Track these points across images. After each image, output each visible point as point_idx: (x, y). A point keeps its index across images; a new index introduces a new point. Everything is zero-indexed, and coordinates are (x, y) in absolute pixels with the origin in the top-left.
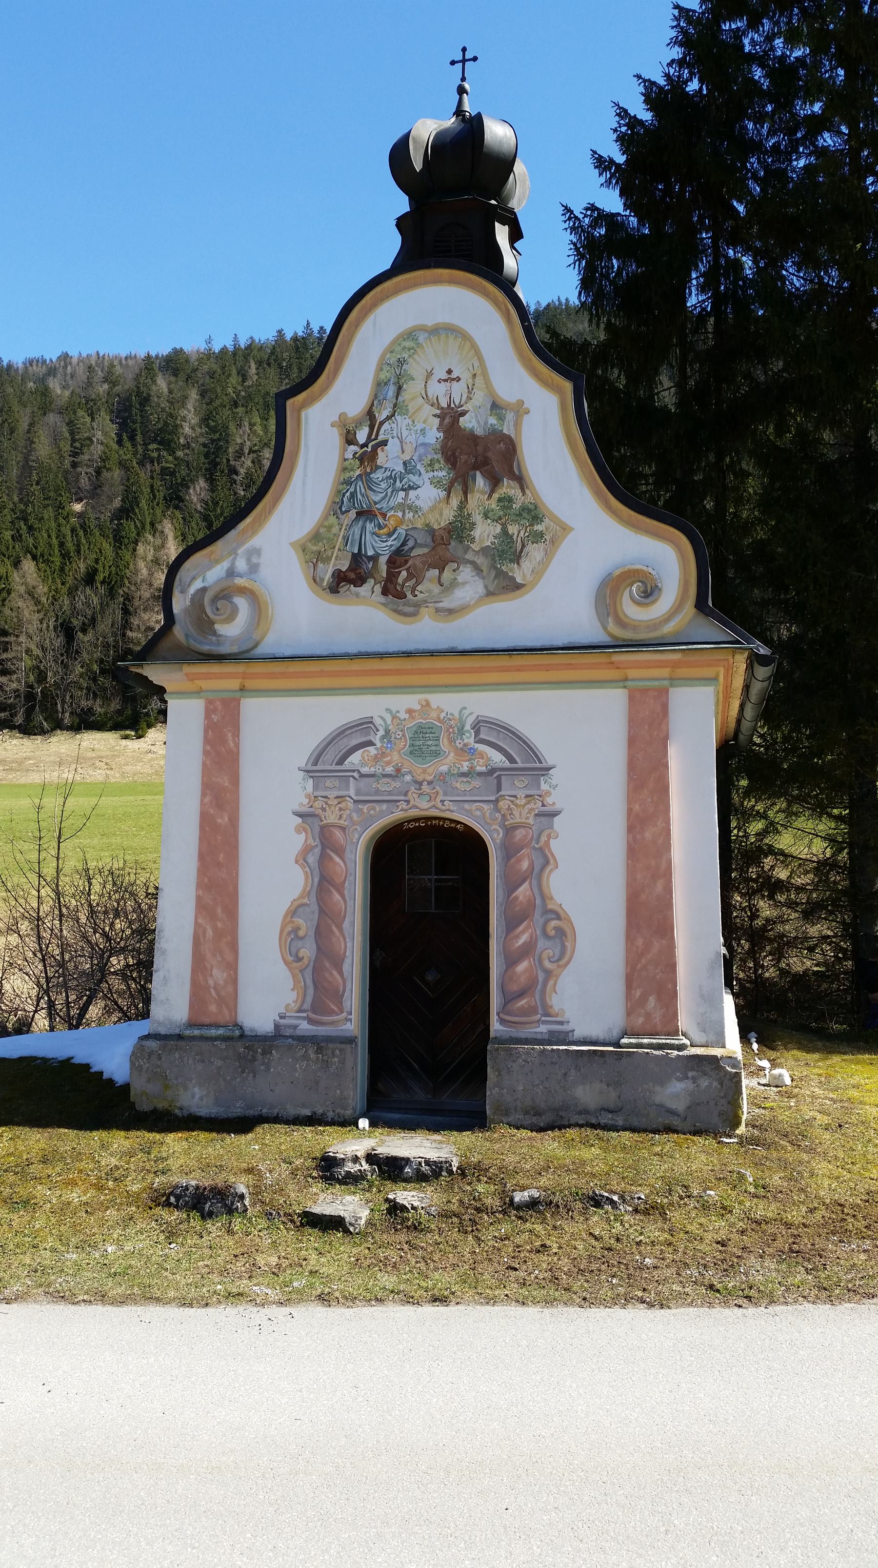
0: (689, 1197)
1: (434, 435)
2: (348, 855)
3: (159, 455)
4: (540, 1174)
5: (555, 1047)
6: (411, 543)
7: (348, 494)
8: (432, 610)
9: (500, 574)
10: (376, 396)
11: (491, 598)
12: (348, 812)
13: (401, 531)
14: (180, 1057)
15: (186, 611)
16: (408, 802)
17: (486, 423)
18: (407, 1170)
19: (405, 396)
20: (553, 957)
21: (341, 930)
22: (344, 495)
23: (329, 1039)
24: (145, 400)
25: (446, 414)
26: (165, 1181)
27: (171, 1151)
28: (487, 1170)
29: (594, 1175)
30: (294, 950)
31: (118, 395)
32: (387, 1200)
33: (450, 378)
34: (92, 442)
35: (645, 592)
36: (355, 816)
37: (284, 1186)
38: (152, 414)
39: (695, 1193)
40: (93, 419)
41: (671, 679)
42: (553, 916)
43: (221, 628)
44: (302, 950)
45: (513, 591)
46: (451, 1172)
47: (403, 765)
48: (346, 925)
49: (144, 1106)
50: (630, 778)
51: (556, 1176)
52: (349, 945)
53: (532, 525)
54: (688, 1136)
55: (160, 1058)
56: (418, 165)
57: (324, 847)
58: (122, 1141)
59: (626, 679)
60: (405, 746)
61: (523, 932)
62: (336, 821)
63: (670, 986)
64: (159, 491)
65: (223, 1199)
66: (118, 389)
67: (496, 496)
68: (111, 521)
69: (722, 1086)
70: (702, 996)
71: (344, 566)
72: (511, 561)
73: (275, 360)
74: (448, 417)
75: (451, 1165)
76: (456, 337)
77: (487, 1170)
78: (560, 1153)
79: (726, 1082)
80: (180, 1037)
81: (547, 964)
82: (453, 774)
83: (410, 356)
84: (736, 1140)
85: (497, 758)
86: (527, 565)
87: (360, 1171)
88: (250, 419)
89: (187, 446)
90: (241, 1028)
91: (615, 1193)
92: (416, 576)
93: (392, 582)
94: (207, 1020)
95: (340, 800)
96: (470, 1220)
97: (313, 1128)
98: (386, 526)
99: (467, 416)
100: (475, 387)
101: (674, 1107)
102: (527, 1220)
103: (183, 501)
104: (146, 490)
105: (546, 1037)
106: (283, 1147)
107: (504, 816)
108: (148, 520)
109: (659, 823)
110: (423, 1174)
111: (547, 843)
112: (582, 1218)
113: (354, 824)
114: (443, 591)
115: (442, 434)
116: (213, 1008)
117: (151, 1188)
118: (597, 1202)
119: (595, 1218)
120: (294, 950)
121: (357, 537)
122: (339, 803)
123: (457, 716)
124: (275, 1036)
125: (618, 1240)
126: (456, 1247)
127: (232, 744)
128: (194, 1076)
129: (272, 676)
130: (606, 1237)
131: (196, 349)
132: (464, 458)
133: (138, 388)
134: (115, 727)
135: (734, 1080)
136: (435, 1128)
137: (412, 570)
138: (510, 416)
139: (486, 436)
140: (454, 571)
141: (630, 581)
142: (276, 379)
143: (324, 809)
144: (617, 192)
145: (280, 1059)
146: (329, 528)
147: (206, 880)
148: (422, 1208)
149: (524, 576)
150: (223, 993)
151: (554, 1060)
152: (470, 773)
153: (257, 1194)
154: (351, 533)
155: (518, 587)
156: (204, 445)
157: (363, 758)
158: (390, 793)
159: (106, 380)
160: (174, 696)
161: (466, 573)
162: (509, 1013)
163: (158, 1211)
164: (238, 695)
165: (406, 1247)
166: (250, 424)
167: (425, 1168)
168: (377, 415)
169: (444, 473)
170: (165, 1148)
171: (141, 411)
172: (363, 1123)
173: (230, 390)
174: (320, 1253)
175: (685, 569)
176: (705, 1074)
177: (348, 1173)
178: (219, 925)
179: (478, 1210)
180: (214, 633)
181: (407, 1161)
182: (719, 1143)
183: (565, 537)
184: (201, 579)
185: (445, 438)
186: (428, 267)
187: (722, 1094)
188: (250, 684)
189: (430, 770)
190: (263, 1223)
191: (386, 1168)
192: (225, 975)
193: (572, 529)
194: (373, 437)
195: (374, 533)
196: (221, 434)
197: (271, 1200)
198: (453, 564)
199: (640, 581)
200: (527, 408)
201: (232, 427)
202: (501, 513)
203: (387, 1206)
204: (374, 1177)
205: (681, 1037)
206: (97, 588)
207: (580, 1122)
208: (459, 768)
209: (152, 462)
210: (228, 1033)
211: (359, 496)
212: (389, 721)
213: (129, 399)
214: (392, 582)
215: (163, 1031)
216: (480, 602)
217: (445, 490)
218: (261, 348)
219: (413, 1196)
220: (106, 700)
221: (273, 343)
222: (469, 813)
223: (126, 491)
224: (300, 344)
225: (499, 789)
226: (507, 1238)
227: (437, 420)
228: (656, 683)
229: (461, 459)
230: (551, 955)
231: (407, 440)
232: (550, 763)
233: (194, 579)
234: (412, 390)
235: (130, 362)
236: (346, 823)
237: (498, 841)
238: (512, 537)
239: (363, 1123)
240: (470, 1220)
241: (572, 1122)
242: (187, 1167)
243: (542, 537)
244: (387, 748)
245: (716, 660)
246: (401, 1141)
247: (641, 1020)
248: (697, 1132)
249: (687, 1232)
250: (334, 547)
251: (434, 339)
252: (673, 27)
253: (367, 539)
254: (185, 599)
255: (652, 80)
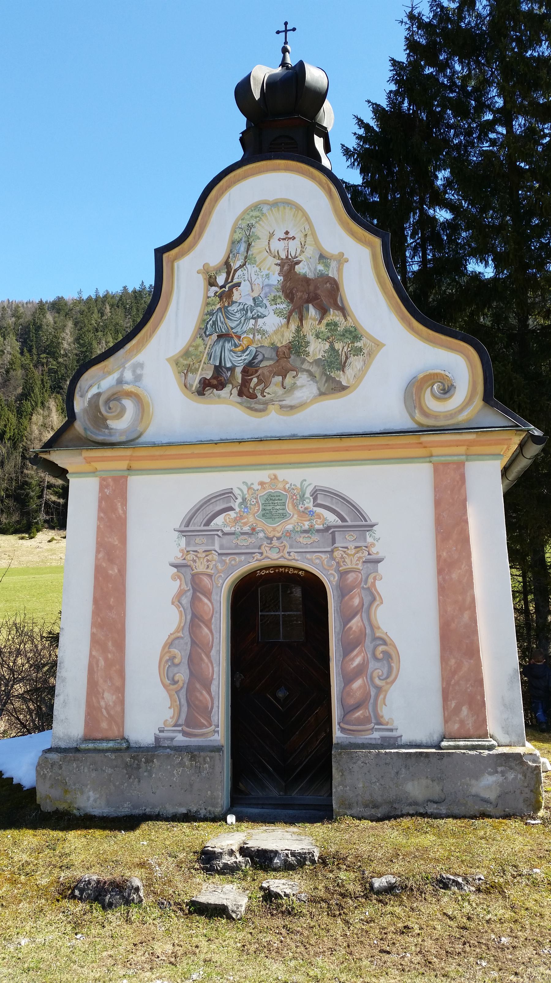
0: (520, 875)
1: (276, 279)
2: (214, 597)
3: (47, 361)
4: (391, 861)
5: (388, 751)
6: (260, 358)
7: (211, 322)
8: (277, 407)
9: (329, 379)
10: (231, 251)
11: (323, 397)
12: (214, 563)
13: (252, 348)
14: (77, 767)
15: (85, 411)
16: (262, 554)
17: (315, 269)
18: (276, 861)
19: (253, 251)
20: (382, 676)
21: (209, 657)
22: (207, 323)
23: (201, 749)
24: (39, 328)
25: (285, 263)
26: (70, 875)
27: (73, 847)
28: (345, 859)
29: (437, 860)
30: (171, 675)
31: (21, 325)
32: (262, 888)
33: (287, 237)
34: (4, 353)
35: (444, 389)
36: (219, 566)
37: (172, 877)
38: (43, 336)
39: (525, 872)
40: (5, 339)
41: (467, 455)
42: (381, 642)
43: (113, 424)
44: (177, 675)
45: (340, 391)
46: (313, 862)
47: (257, 525)
48: (213, 653)
49: (47, 807)
50: (438, 532)
51: (406, 863)
52: (216, 669)
53: (353, 342)
54: (501, 820)
55: (60, 767)
56: (257, 96)
57: (195, 590)
58: (31, 839)
59: (431, 456)
60: (258, 510)
61: (357, 656)
62: (205, 570)
63: (479, 698)
64: (47, 383)
65: (121, 892)
66: (21, 321)
67: (324, 322)
68: (16, 401)
69: (525, 778)
70: (505, 705)
71: (209, 375)
72: (338, 369)
73: (122, 304)
74: (286, 265)
75: (313, 856)
76: (291, 208)
77: (345, 859)
78: (402, 840)
79: (529, 774)
80: (77, 750)
81: (377, 682)
82: (297, 532)
83: (257, 222)
84: (540, 822)
85: (332, 518)
86: (350, 372)
87: (236, 862)
88: (106, 339)
89: (66, 355)
90: (127, 741)
91: (459, 875)
92: (264, 382)
93: (246, 387)
94: (99, 735)
95: (208, 553)
96: (337, 904)
97: (189, 824)
98: (240, 345)
99: (301, 265)
100: (306, 244)
101: (487, 796)
102: (387, 903)
103: (62, 389)
104: (39, 382)
105: (379, 742)
106: (167, 843)
107: (338, 563)
108: (40, 402)
109: (463, 566)
110: (290, 864)
111: (374, 584)
112: (434, 900)
113: (219, 572)
114: (285, 393)
115: (282, 278)
116: (104, 725)
117: (58, 882)
118: (444, 884)
119: (446, 899)
120: (171, 675)
121: (218, 354)
122: (207, 556)
123: (299, 486)
124: (155, 747)
125: (469, 919)
126: (328, 931)
127: (121, 511)
128: (89, 782)
129: (153, 458)
130: (459, 916)
131: (71, 298)
132: (299, 294)
133: (34, 320)
134: (15, 532)
135: (535, 772)
136: (291, 821)
137: (261, 377)
138: (334, 264)
139: (316, 279)
140: (294, 377)
141: (430, 382)
142: (123, 315)
143: (194, 561)
144: (359, 171)
145: (160, 766)
146: (197, 347)
147: (99, 620)
148: (294, 895)
149: (348, 381)
150: (112, 713)
151: (388, 761)
152: (310, 530)
153: (150, 885)
154: (213, 350)
155: (344, 388)
156: (76, 355)
157: (226, 520)
158: (247, 547)
159: (13, 316)
160: (74, 475)
161: (303, 378)
162: (347, 723)
163: (65, 903)
164: (126, 473)
165: (283, 931)
166: (106, 342)
167: (291, 859)
168: (232, 265)
169: (284, 306)
170: (67, 844)
171: (36, 334)
172: (231, 819)
173: (93, 322)
174: (209, 940)
175: (473, 372)
176: (511, 768)
177: (226, 865)
178: (110, 656)
179: (343, 895)
180: (107, 427)
181: (276, 853)
182: (526, 824)
183: (378, 351)
184: (96, 386)
185: (284, 280)
186: (270, 159)
187: (526, 784)
188: (136, 465)
189: (279, 529)
190: (157, 912)
191: (258, 860)
192: (114, 697)
193: (384, 345)
194: (230, 280)
195: (231, 351)
196: (87, 348)
197: (162, 891)
198: (292, 372)
199: (439, 382)
200: (346, 258)
201: (95, 343)
202: (329, 334)
203: (262, 893)
204: (248, 867)
205: (491, 739)
206: (5, 443)
207: (411, 812)
208: (301, 527)
209: (43, 365)
210: (117, 746)
211: (219, 324)
212: (245, 492)
213: (28, 327)
214: (246, 387)
215: (63, 745)
216: (315, 400)
217: (285, 318)
218: (113, 297)
219: (283, 884)
220: (9, 514)
221: (121, 294)
222: (311, 561)
223: (25, 383)
224: (137, 295)
225: (334, 542)
226: (372, 921)
227: (278, 268)
228: (456, 458)
229: (297, 295)
230: (380, 674)
231: (256, 282)
232: (374, 521)
233: (91, 386)
234: (258, 247)
235: (29, 306)
236: (212, 572)
237: (334, 583)
238: (337, 351)
239: (231, 819)
240: (337, 904)
241: (404, 812)
242: (87, 862)
243: (361, 351)
244: (244, 512)
245: (503, 440)
246: (265, 834)
247: (457, 726)
248: (507, 816)
249: (527, 909)
250: (201, 361)
251: (274, 210)
252: (391, 71)
253: (226, 354)
254: (84, 402)
255: (378, 103)
